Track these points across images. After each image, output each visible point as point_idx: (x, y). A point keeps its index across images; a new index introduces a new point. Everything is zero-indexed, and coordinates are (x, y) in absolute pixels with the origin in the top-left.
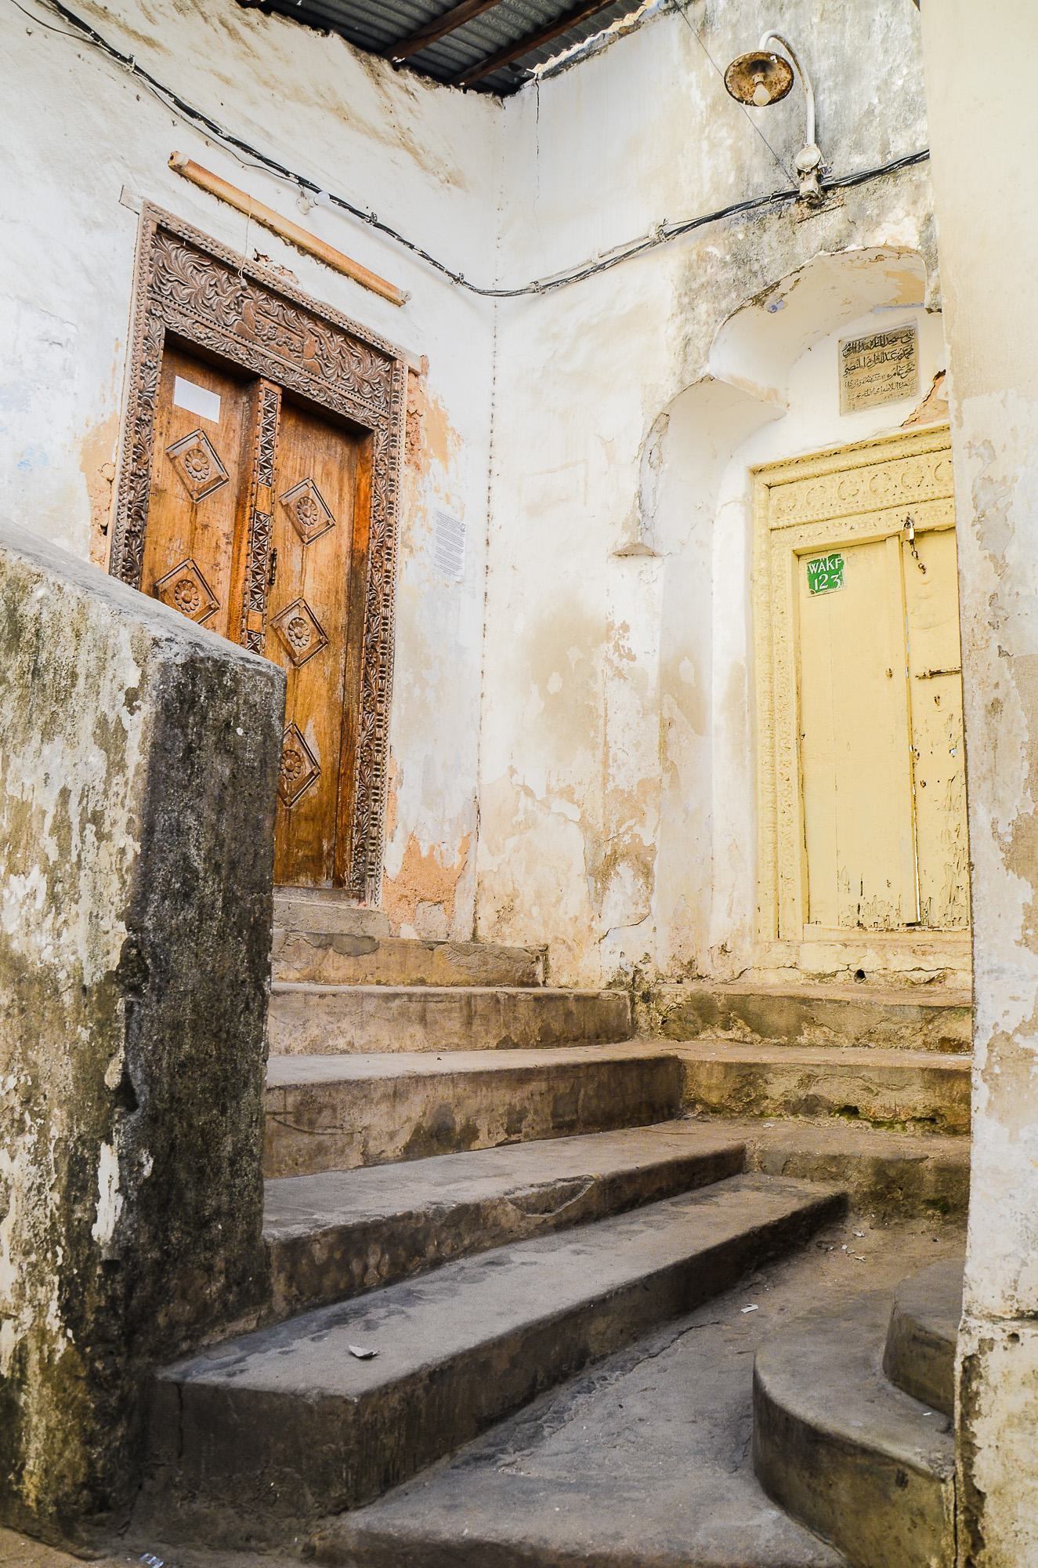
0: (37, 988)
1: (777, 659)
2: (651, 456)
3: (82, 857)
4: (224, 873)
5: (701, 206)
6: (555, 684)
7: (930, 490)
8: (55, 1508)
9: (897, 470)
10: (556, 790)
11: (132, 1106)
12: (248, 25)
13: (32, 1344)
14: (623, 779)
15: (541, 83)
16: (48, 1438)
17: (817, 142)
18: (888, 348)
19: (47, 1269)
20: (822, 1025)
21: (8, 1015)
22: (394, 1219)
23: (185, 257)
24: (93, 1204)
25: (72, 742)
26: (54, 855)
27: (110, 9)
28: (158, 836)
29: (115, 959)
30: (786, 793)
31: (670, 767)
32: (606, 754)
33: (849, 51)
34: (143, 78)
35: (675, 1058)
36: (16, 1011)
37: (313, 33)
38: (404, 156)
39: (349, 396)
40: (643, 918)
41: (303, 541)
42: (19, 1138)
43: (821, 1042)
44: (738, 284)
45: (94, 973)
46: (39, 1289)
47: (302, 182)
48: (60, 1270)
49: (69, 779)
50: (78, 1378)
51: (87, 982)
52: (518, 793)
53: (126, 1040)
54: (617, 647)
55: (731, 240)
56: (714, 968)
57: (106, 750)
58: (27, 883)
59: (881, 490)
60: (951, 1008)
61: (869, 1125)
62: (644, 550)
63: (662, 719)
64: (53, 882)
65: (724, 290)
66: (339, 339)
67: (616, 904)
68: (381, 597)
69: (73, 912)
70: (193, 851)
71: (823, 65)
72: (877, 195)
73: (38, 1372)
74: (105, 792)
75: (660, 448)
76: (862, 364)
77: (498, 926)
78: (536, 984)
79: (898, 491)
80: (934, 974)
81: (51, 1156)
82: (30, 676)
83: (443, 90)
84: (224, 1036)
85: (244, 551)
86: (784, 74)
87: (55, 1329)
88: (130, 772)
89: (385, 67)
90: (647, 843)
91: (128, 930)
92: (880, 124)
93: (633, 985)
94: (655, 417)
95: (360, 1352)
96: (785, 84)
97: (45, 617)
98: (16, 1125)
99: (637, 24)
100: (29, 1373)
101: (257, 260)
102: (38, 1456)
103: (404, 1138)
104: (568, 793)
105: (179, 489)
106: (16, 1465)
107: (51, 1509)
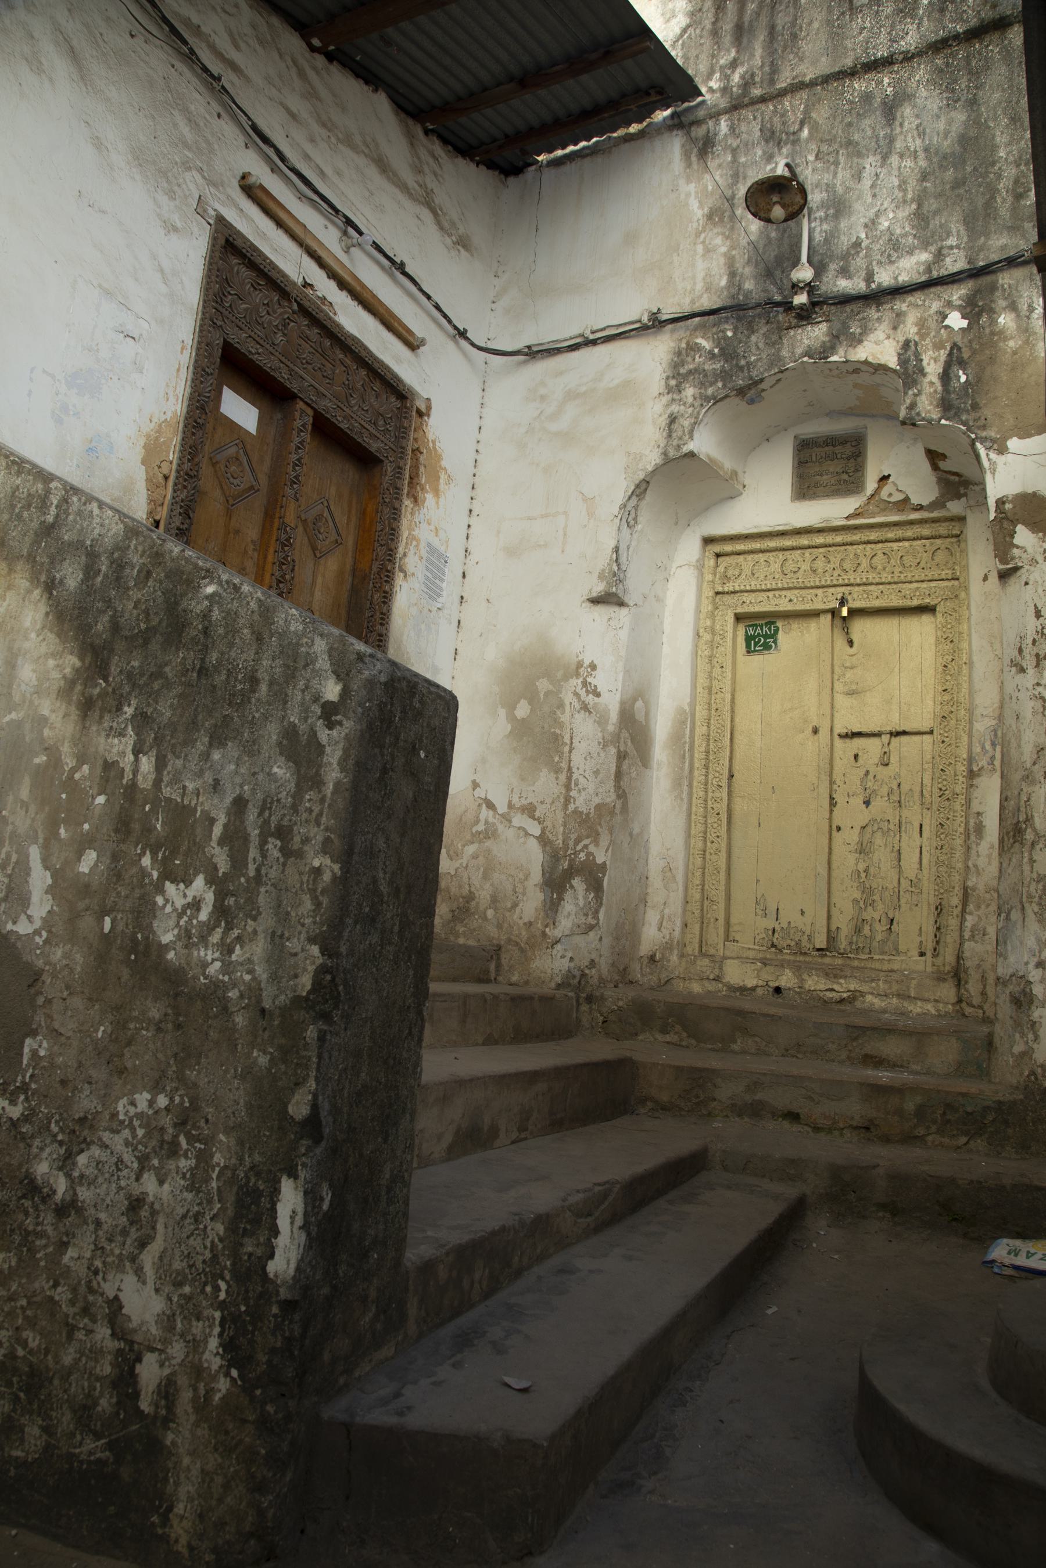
0: (199, 1004)
1: (714, 706)
2: (629, 517)
3: (263, 872)
4: (402, 897)
5: (693, 302)
6: (523, 710)
7: (864, 575)
8: (213, 1557)
9: (836, 556)
10: (517, 806)
11: (317, 1139)
12: (314, 68)
13: (182, 1381)
14: (582, 802)
15: (546, 171)
16: (203, 1481)
17: (809, 261)
18: (838, 449)
19: (204, 1304)
20: (754, 1035)
21: (159, 1029)
22: (494, 1233)
23: (245, 273)
24: (269, 1240)
25: (251, 749)
26: (223, 864)
27: (203, 29)
28: (356, 858)
29: (305, 982)
30: (715, 825)
31: (622, 794)
32: (569, 778)
33: (840, 190)
34: (226, 98)
35: (631, 1059)
36: (170, 1026)
37: (365, 88)
38: (426, 215)
39: (367, 426)
40: (591, 928)
41: (315, 556)
42: (171, 1162)
43: (753, 1051)
44: (724, 376)
45: (276, 997)
46: (194, 1323)
47: (349, 222)
48: (222, 1306)
49: (246, 788)
50: (244, 1421)
51: (267, 1004)
52: (480, 805)
53: (318, 1069)
54: (585, 684)
55: (721, 335)
56: (643, 975)
57: (296, 763)
58: (187, 892)
59: (820, 570)
60: (874, 1029)
61: (809, 1129)
62: (615, 600)
63: (619, 751)
64: (221, 896)
65: (711, 378)
66: (363, 372)
67: (569, 914)
68: (378, 615)
69: (250, 929)
70: (381, 875)
71: (815, 197)
72: (860, 316)
73: (190, 1410)
74: (295, 808)
75: (636, 510)
76: (814, 459)
77: (452, 924)
78: (488, 981)
80: (845, 995)
81: (214, 1184)
82: (195, 675)
83: (461, 162)
84: (391, 1062)
85: (270, 558)
86: (798, 199)
87: (215, 1367)
88: (329, 788)
89: (419, 131)
91: (323, 955)
92: (866, 256)
93: (579, 988)
94: (637, 482)
95: (517, 1384)
96: (796, 208)
97: (216, 614)
98: (166, 1147)
99: (641, 134)
100: (179, 1410)
101: (304, 286)
102: (190, 1499)
103: (448, 1139)
104: (529, 810)
105: (217, 493)
106: (160, 1507)
107: (209, 1557)
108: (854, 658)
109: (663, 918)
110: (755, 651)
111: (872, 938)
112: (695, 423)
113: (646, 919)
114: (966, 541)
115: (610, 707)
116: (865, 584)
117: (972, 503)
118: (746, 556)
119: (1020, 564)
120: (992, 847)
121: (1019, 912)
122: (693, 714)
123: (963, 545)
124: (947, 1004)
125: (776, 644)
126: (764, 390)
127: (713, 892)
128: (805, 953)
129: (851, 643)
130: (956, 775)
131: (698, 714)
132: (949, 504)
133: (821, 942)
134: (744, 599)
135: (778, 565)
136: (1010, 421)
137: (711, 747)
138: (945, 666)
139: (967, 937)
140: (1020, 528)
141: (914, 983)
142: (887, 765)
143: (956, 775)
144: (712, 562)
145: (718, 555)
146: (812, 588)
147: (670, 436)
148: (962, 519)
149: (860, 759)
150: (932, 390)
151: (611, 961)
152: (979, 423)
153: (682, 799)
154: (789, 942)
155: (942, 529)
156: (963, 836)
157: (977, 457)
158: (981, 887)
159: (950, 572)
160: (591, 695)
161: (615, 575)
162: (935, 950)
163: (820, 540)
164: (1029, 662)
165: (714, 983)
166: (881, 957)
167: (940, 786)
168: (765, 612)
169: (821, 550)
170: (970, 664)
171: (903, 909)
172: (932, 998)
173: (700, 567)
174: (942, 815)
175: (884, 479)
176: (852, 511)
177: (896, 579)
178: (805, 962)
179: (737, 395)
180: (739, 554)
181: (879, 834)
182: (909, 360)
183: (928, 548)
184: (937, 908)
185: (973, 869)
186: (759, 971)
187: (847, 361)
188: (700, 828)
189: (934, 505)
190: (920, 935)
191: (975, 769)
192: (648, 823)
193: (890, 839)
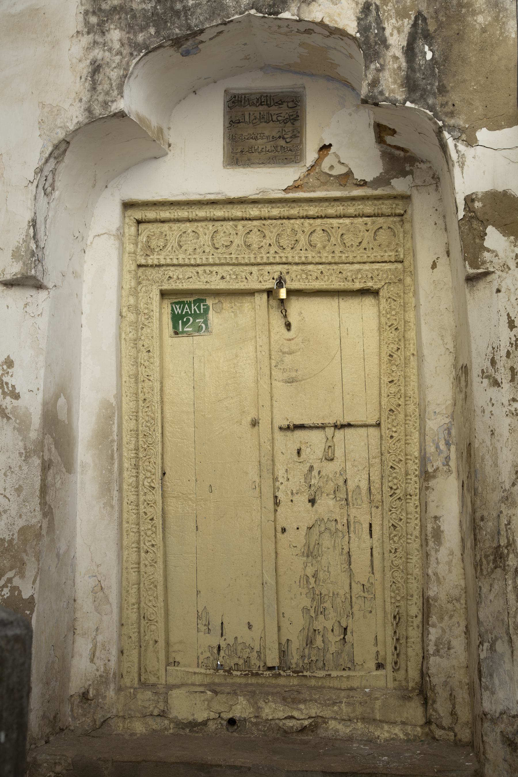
1: (141, 396)
18: (274, 110)
30: (149, 533)
56: (74, 718)
62: (32, 282)
63: (43, 462)
76: (247, 119)
79: (272, 250)
80: (306, 723)
90: (26, 595)
94: (56, 142)
108: (292, 342)
109: (95, 646)
110: (183, 332)
111: (325, 650)
112: (125, 76)
113: (76, 650)
114: (411, 221)
115: (32, 410)
116: (304, 263)
117: (419, 182)
118: (171, 224)
119: (491, 269)
120: (452, 553)
121: (506, 644)
122: (120, 408)
123: (407, 226)
124: (415, 726)
125: (207, 325)
126: (202, 42)
127: (151, 610)
128: (257, 674)
129: (288, 326)
130: (407, 474)
131: (124, 406)
132: (394, 182)
133: (273, 659)
134: (171, 274)
135: (208, 237)
136: (479, 109)
137: (141, 443)
138: (391, 356)
139: (431, 652)
140: (490, 230)
141: (378, 703)
142: (332, 460)
143: (407, 474)
144: (133, 230)
145: (139, 222)
146: (246, 265)
147: (94, 88)
148: (406, 198)
149: (303, 453)
150: (396, 66)
151: (41, 713)
152: (446, 109)
153: (112, 507)
154: (236, 660)
155: (385, 207)
156: (418, 540)
157: (444, 147)
158: (443, 596)
159: (393, 254)
160: (8, 398)
161: (33, 254)
162: (396, 663)
163: (254, 212)
164: (503, 376)
165: (159, 719)
166: (340, 673)
167: (390, 484)
168: (195, 290)
169: (255, 223)
170: (420, 357)
171: (356, 617)
172: (399, 720)
173: (120, 236)
174: (394, 516)
175: (325, 148)
176: (291, 183)
177: (337, 260)
178: (258, 684)
179: (171, 46)
180: (163, 221)
181: (327, 535)
182: (370, 26)
183: (369, 226)
184: (395, 617)
185: (433, 578)
186: (210, 701)
187: (300, 20)
188: (133, 537)
189: (378, 182)
190: (376, 644)
191: (430, 470)
192: (74, 537)
193: (338, 540)
